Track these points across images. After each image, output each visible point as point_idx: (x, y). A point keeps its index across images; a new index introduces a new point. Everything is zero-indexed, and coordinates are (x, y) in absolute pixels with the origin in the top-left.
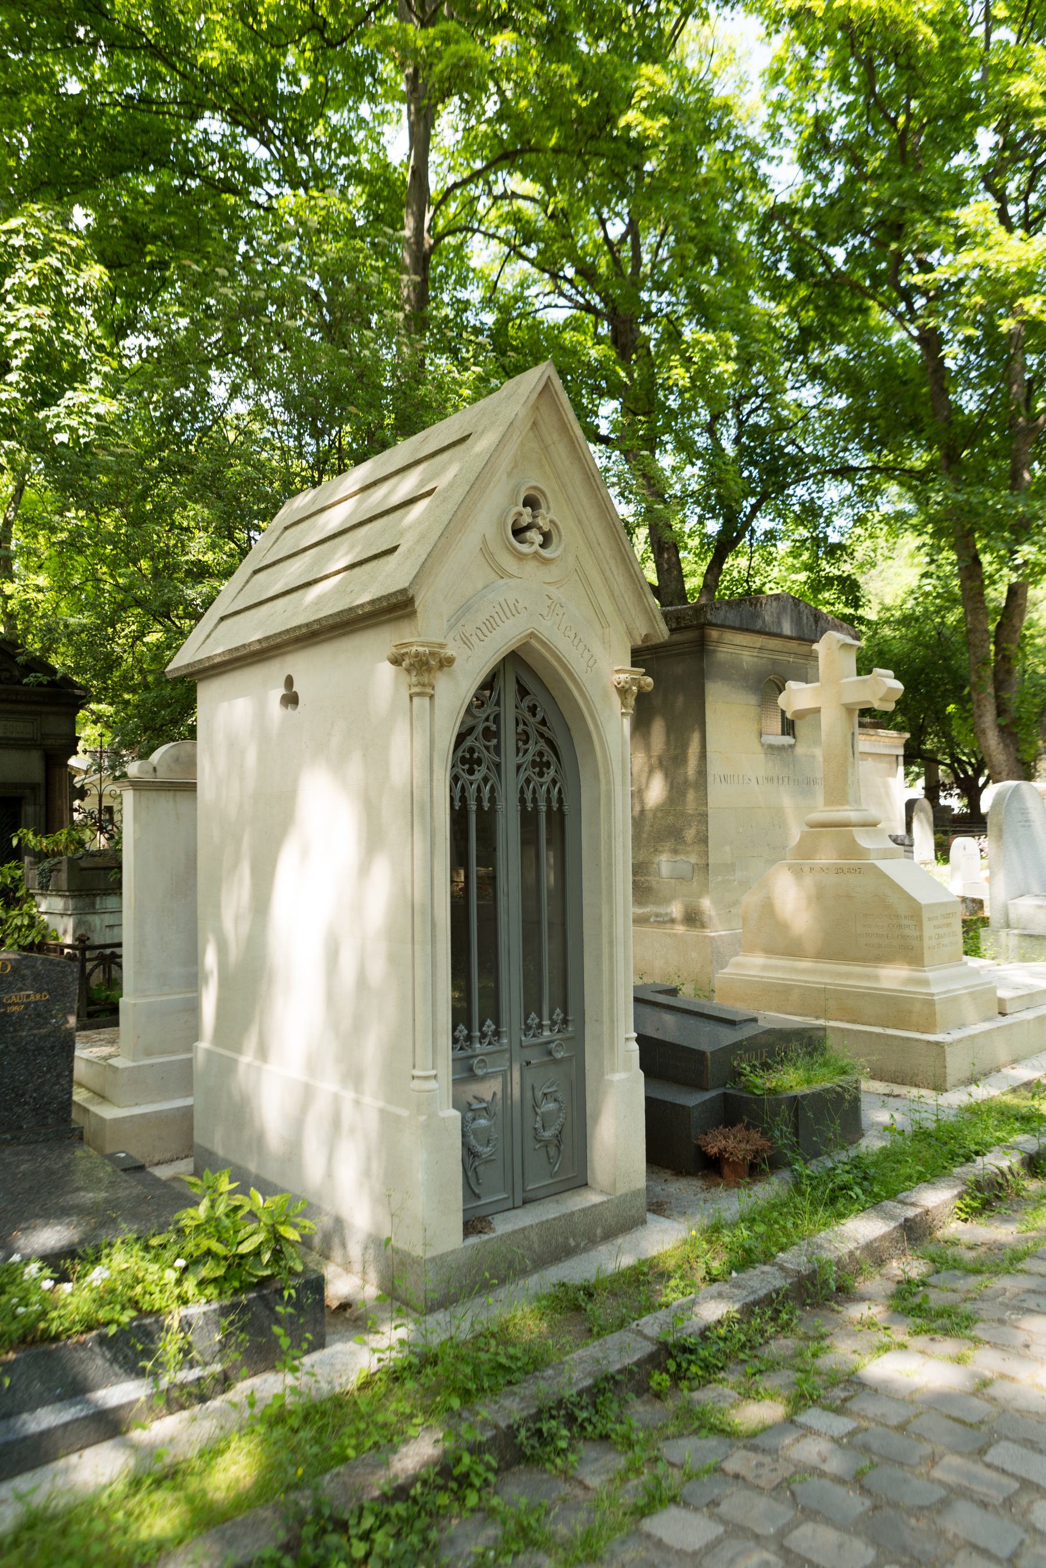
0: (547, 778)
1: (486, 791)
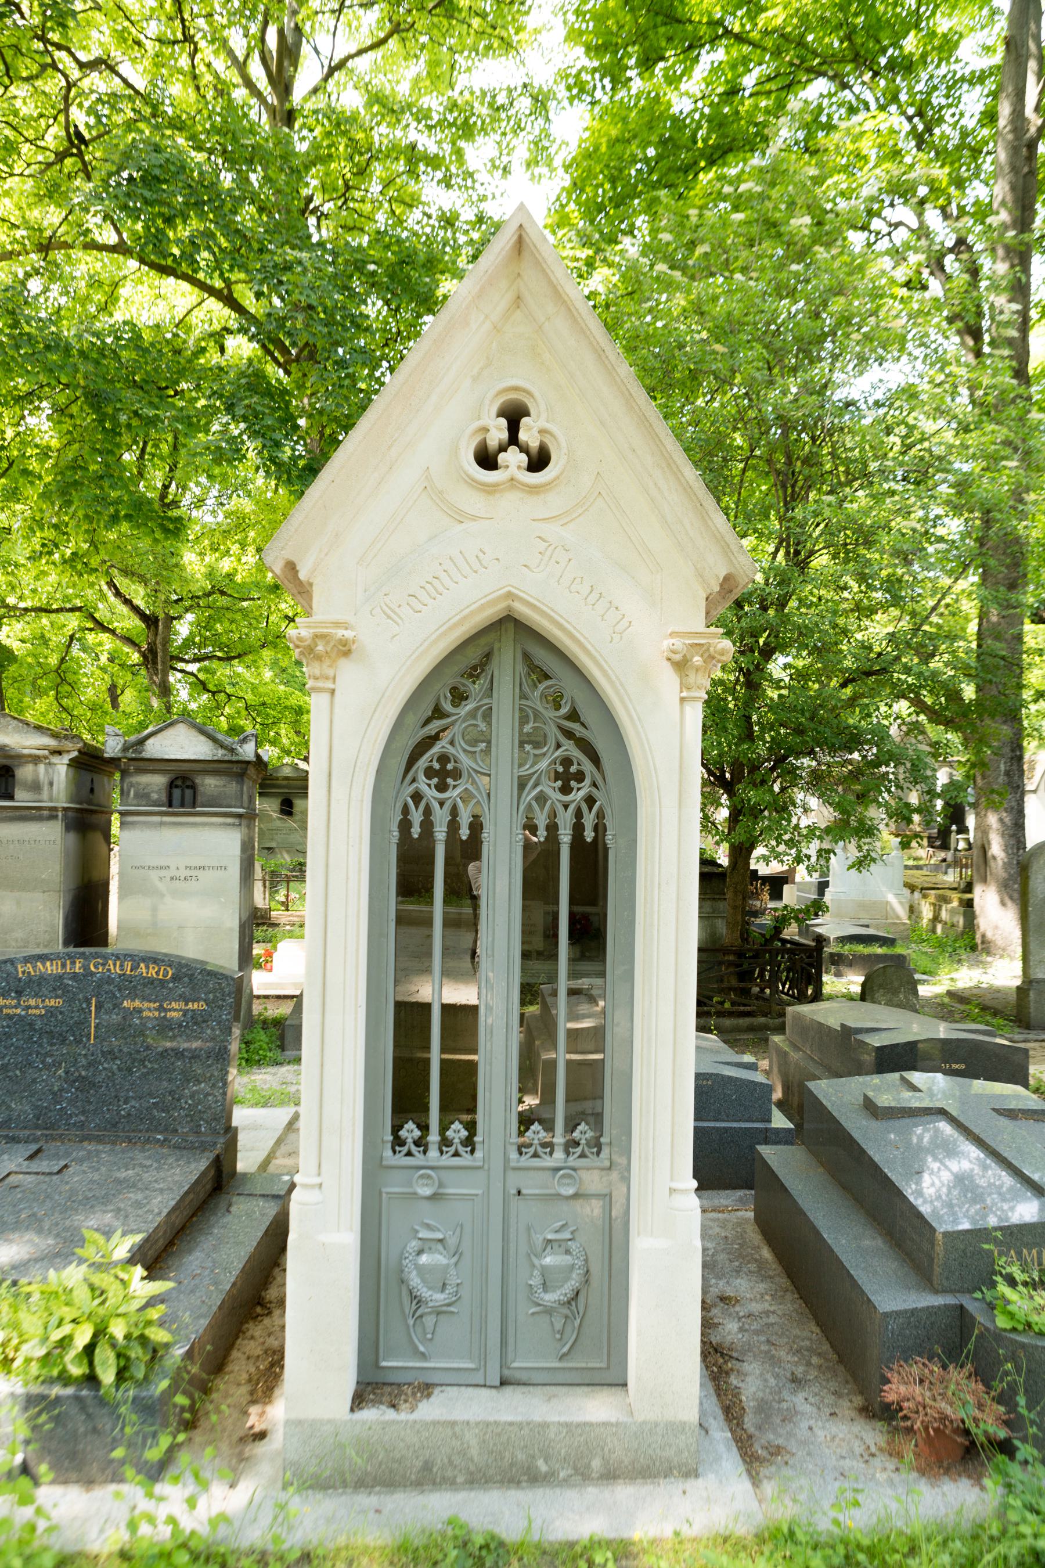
0: (577, 796)
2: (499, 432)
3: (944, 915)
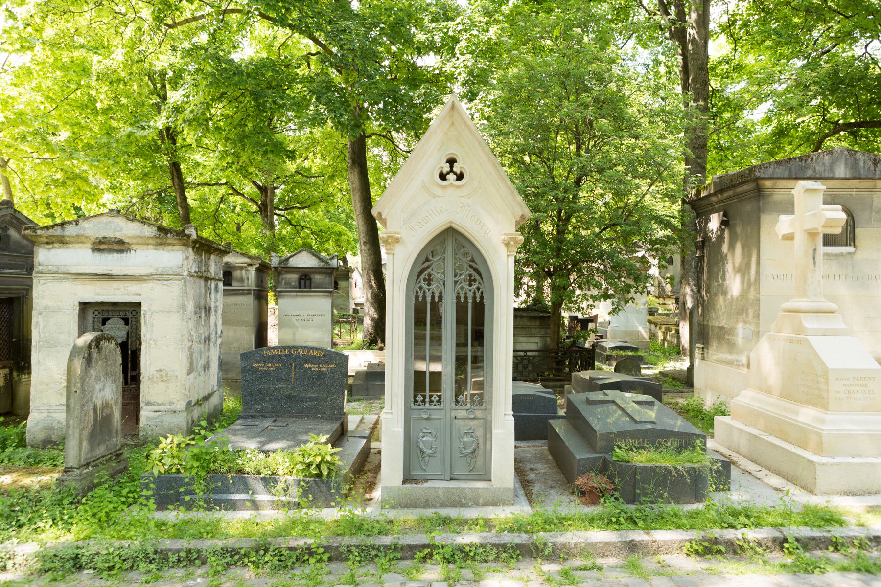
0: (474, 287)
1: (478, 295)
2: (447, 168)
3: (668, 338)
